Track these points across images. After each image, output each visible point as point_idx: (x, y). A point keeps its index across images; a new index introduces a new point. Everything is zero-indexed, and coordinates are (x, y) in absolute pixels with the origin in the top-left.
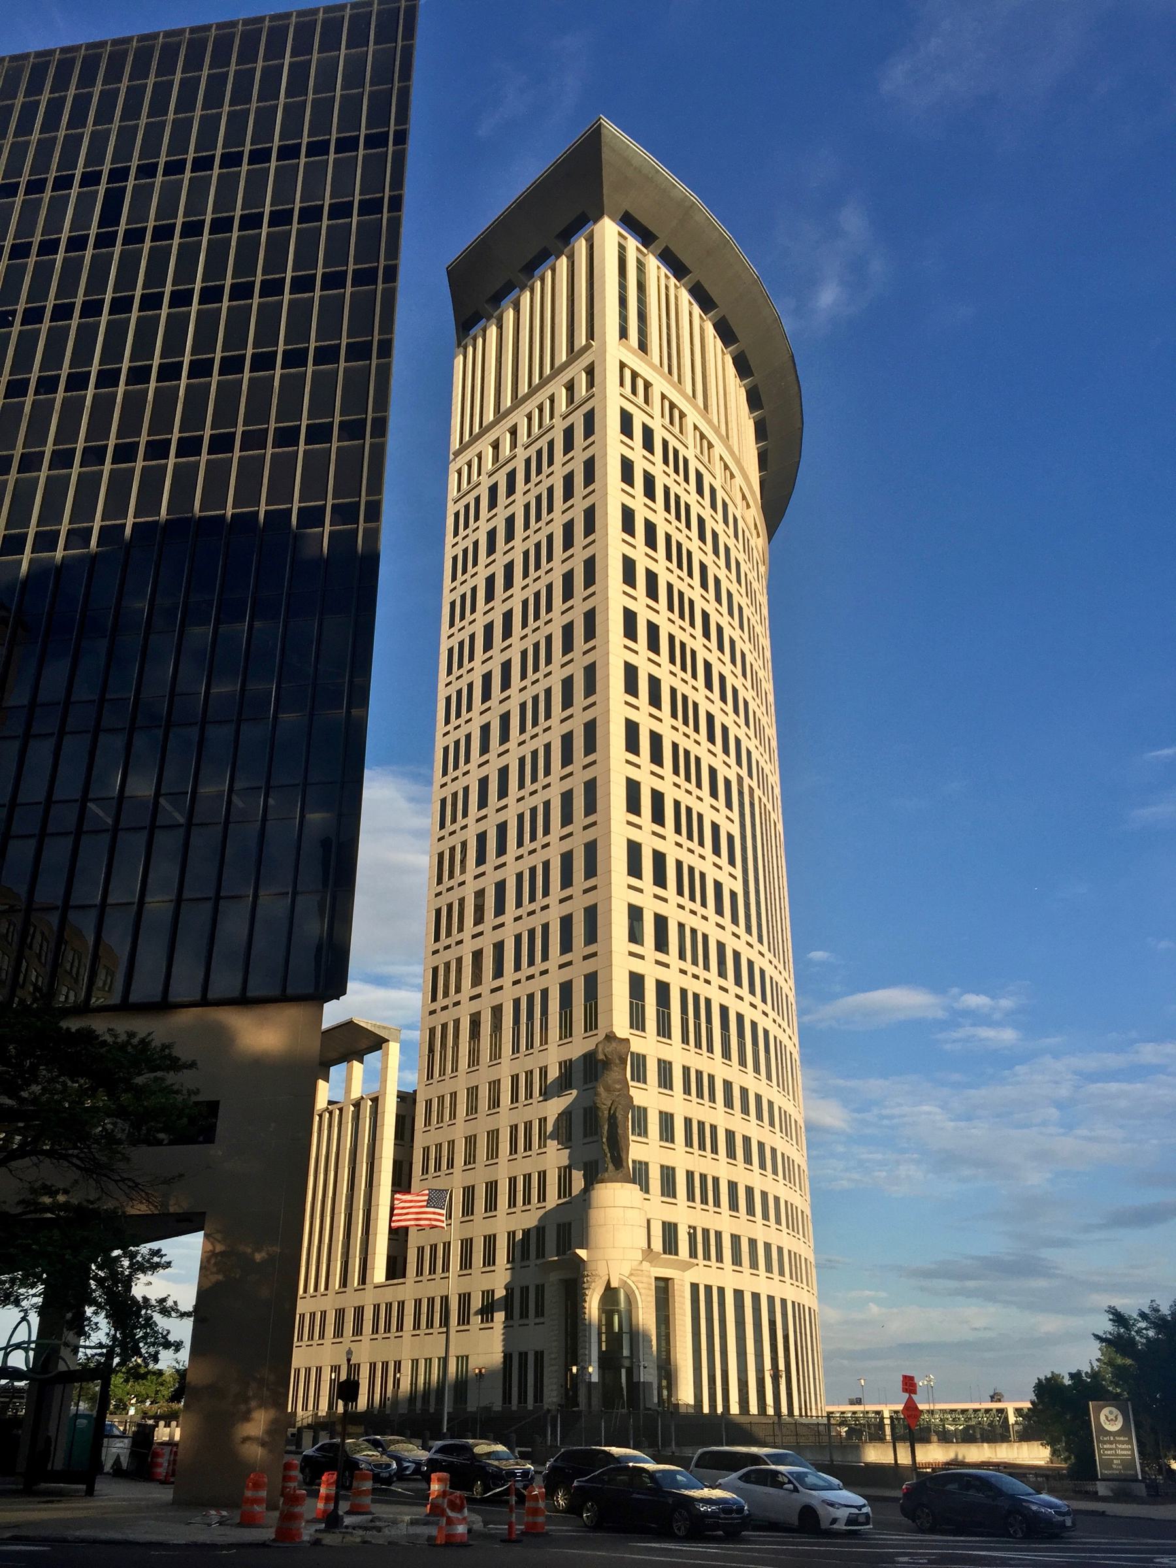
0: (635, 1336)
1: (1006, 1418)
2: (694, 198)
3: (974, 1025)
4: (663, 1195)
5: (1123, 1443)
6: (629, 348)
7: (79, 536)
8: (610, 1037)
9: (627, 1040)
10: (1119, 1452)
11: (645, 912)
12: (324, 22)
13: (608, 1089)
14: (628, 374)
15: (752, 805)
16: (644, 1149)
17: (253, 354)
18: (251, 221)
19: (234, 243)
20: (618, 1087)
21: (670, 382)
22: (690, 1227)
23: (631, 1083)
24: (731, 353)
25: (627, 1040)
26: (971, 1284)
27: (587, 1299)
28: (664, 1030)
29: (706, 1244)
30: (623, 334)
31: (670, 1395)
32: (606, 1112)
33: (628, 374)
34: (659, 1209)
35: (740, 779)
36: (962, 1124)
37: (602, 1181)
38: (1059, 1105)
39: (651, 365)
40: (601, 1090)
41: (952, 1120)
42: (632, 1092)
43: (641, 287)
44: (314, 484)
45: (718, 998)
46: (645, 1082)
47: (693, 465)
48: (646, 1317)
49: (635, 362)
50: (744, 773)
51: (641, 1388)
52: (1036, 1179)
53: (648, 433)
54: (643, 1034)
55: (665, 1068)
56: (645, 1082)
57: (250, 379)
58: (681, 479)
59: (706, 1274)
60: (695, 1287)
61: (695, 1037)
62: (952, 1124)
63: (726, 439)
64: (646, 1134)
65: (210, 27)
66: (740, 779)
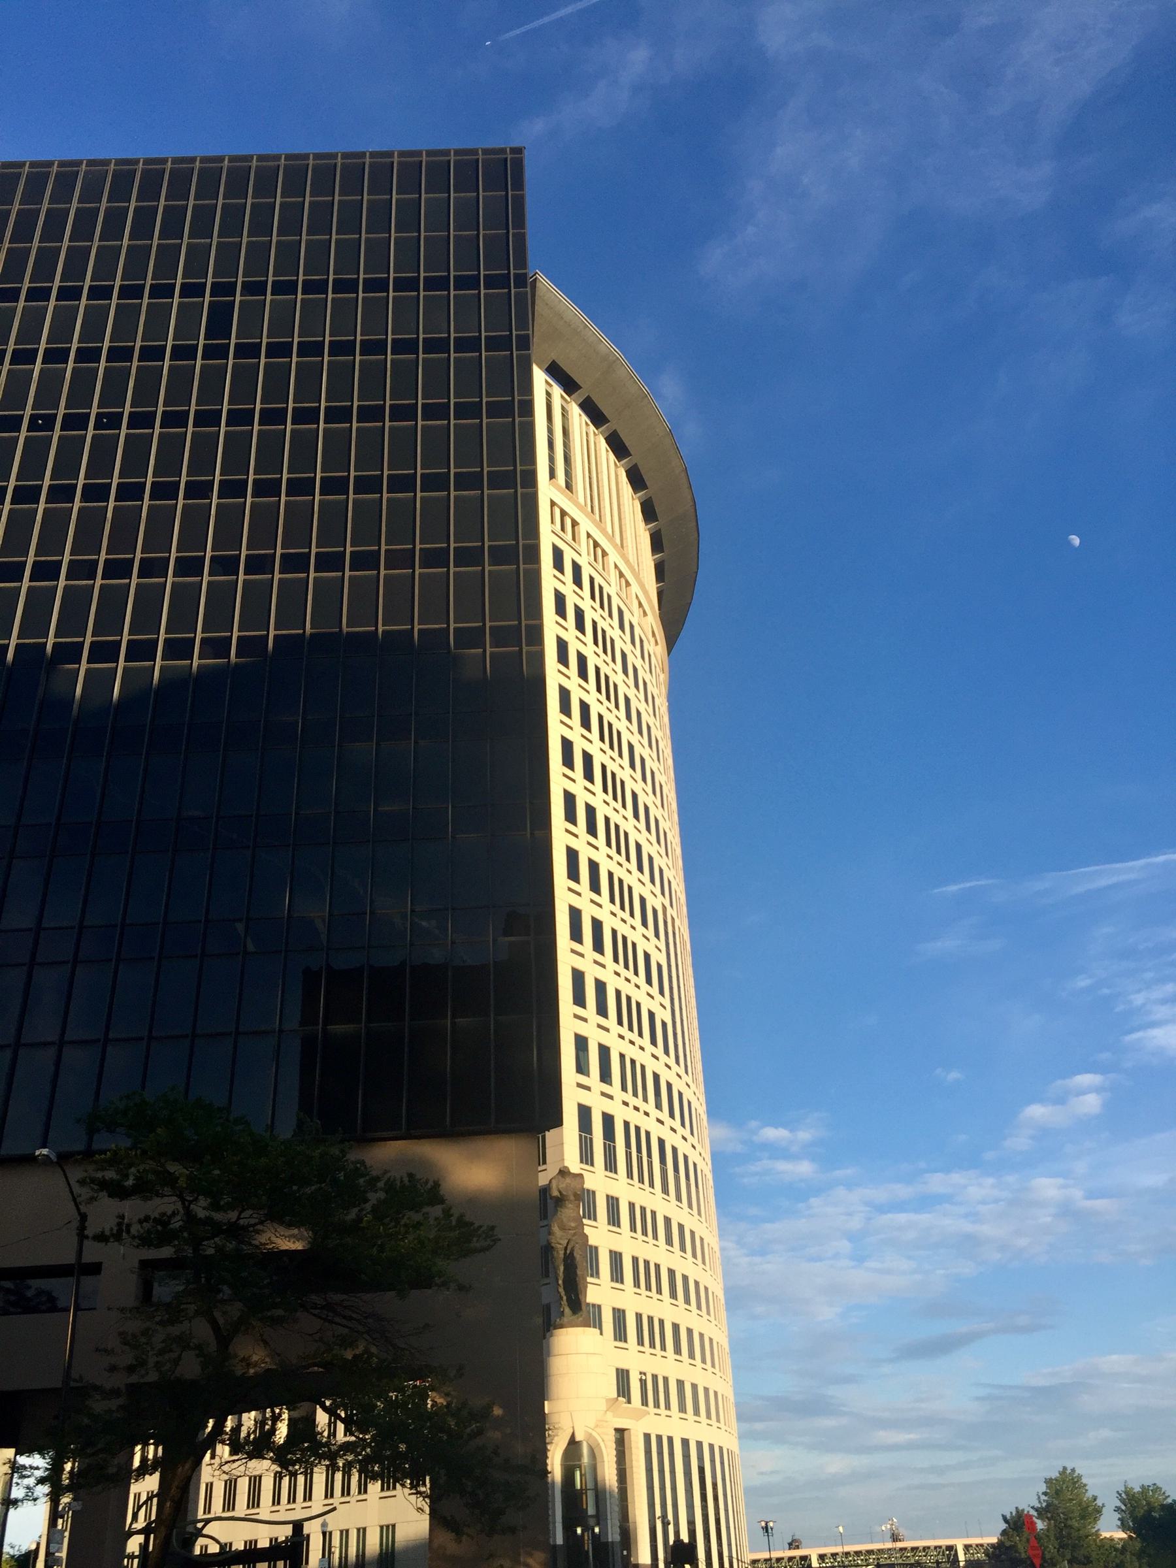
0: (600, 1493)
1: (956, 1554)
2: (617, 353)
3: (770, 1158)
4: (615, 1339)
6: (558, 488)
7: (215, 647)
8: (564, 1172)
9: (581, 1176)
11: (590, 1041)
12: (201, 169)
13: (563, 1228)
15: (674, 934)
16: (599, 1291)
17: (119, 484)
18: (153, 353)
19: (165, 372)
20: (573, 1225)
21: (594, 521)
23: (585, 1221)
24: (639, 498)
25: (581, 1176)
26: (759, 1426)
27: (549, 1454)
28: (611, 1165)
29: (655, 1391)
30: (552, 475)
31: (629, 1555)
32: (562, 1253)
35: (664, 908)
36: (757, 1259)
37: (562, 1327)
38: (851, 1237)
39: (577, 504)
40: (555, 1229)
41: (748, 1256)
42: (587, 1230)
43: (566, 432)
44: (73, 620)
45: (657, 1131)
46: (595, 1220)
47: (615, 601)
48: (609, 1475)
49: (563, 502)
50: (667, 904)
52: (827, 1314)
53: (577, 568)
56: (595, 1220)
57: (115, 507)
58: (606, 615)
60: (647, 1437)
61: (639, 1173)
62: (747, 1259)
63: (637, 575)
64: (598, 1275)
65: (81, 162)
66: (664, 908)
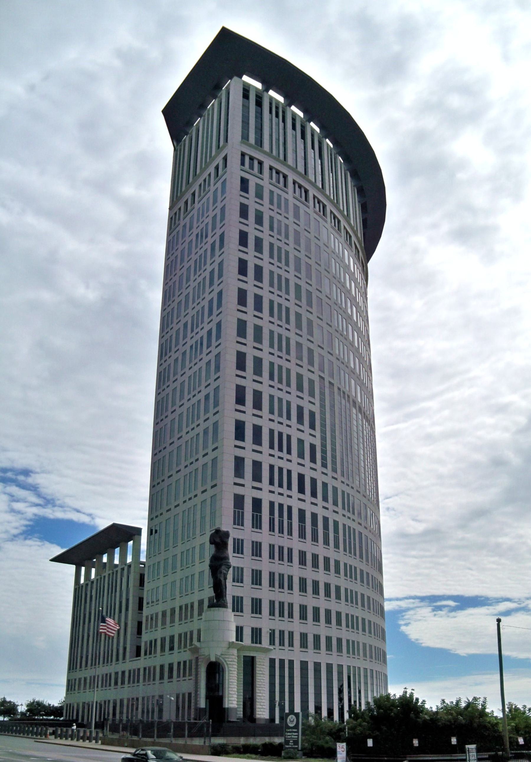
5: (295, 732)
10: (293, 737)
14: (247, 159)
22: (270, 630)
33: (247, 159)
34: (248, 621)
51: (226, 711)
54: (304, 541)
55: (302, 555)
59: (334, 659)
63: (336, 205)
